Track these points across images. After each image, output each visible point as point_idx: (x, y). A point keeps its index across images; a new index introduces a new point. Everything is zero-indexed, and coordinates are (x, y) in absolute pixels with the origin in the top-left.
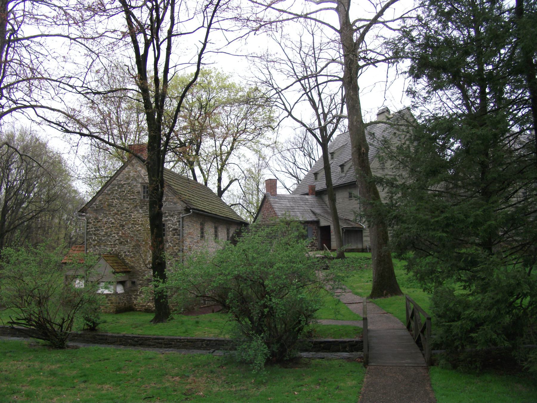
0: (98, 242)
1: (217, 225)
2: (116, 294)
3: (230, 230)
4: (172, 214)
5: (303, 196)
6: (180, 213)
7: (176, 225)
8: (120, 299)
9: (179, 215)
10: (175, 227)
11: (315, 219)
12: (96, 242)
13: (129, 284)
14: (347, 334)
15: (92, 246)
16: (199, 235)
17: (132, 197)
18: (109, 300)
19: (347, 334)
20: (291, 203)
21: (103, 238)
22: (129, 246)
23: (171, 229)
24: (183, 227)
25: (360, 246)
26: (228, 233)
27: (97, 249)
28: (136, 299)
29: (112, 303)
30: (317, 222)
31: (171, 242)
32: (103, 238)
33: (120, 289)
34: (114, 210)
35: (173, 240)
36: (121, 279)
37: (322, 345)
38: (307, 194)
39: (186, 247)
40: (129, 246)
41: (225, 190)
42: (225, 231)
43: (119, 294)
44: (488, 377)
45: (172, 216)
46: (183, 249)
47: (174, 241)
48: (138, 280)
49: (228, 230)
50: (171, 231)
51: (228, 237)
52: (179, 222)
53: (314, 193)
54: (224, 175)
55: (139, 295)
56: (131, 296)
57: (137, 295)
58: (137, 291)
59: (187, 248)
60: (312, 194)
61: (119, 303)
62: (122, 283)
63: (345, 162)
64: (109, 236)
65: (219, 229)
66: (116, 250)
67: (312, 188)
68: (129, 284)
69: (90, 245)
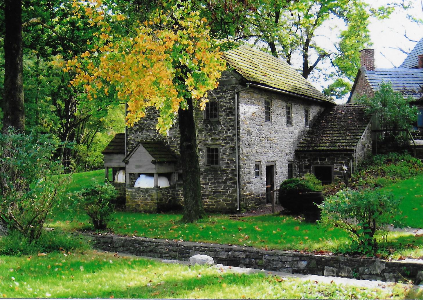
0: (140, 127)
1: (289, 105)
2: (157, 188)
3: (310, 112)
4: (224, 90)
5: (411, 70)
6: (234, 88)
7: (230, 102)
8: (163, 195)
9: (234, 90)
10: (229, 105)
12: (137, 127)
14: (140, 262)
15: (133, 131)
16: (264, 117)
18: (149, 196)
19: (165, 262)
20: (394, 79)
21: (145, 122)
22: (175, 131)
23: (224, 108)
26: (306, 116)
27: (139, 135)
29: (152, 200)
31: (224, 124)
32: (145, 122)
33: (164, 183)
35: (226, 122)
38: (417, 67)
40: (175, 131)
41: (312, 68)
42: (303, 112)
43: (162, 189)
44: (256, 96)
45: (225, 92)
47: (228, 123)
49: (307, 112)
50: (224, 111)
51: (307, 120)
52: (234, 98)
54: (311, 52)
59: (244, 132)
62: (168, 176)
64: (152, 119)
65: (294, 110)
69: (131, 131)
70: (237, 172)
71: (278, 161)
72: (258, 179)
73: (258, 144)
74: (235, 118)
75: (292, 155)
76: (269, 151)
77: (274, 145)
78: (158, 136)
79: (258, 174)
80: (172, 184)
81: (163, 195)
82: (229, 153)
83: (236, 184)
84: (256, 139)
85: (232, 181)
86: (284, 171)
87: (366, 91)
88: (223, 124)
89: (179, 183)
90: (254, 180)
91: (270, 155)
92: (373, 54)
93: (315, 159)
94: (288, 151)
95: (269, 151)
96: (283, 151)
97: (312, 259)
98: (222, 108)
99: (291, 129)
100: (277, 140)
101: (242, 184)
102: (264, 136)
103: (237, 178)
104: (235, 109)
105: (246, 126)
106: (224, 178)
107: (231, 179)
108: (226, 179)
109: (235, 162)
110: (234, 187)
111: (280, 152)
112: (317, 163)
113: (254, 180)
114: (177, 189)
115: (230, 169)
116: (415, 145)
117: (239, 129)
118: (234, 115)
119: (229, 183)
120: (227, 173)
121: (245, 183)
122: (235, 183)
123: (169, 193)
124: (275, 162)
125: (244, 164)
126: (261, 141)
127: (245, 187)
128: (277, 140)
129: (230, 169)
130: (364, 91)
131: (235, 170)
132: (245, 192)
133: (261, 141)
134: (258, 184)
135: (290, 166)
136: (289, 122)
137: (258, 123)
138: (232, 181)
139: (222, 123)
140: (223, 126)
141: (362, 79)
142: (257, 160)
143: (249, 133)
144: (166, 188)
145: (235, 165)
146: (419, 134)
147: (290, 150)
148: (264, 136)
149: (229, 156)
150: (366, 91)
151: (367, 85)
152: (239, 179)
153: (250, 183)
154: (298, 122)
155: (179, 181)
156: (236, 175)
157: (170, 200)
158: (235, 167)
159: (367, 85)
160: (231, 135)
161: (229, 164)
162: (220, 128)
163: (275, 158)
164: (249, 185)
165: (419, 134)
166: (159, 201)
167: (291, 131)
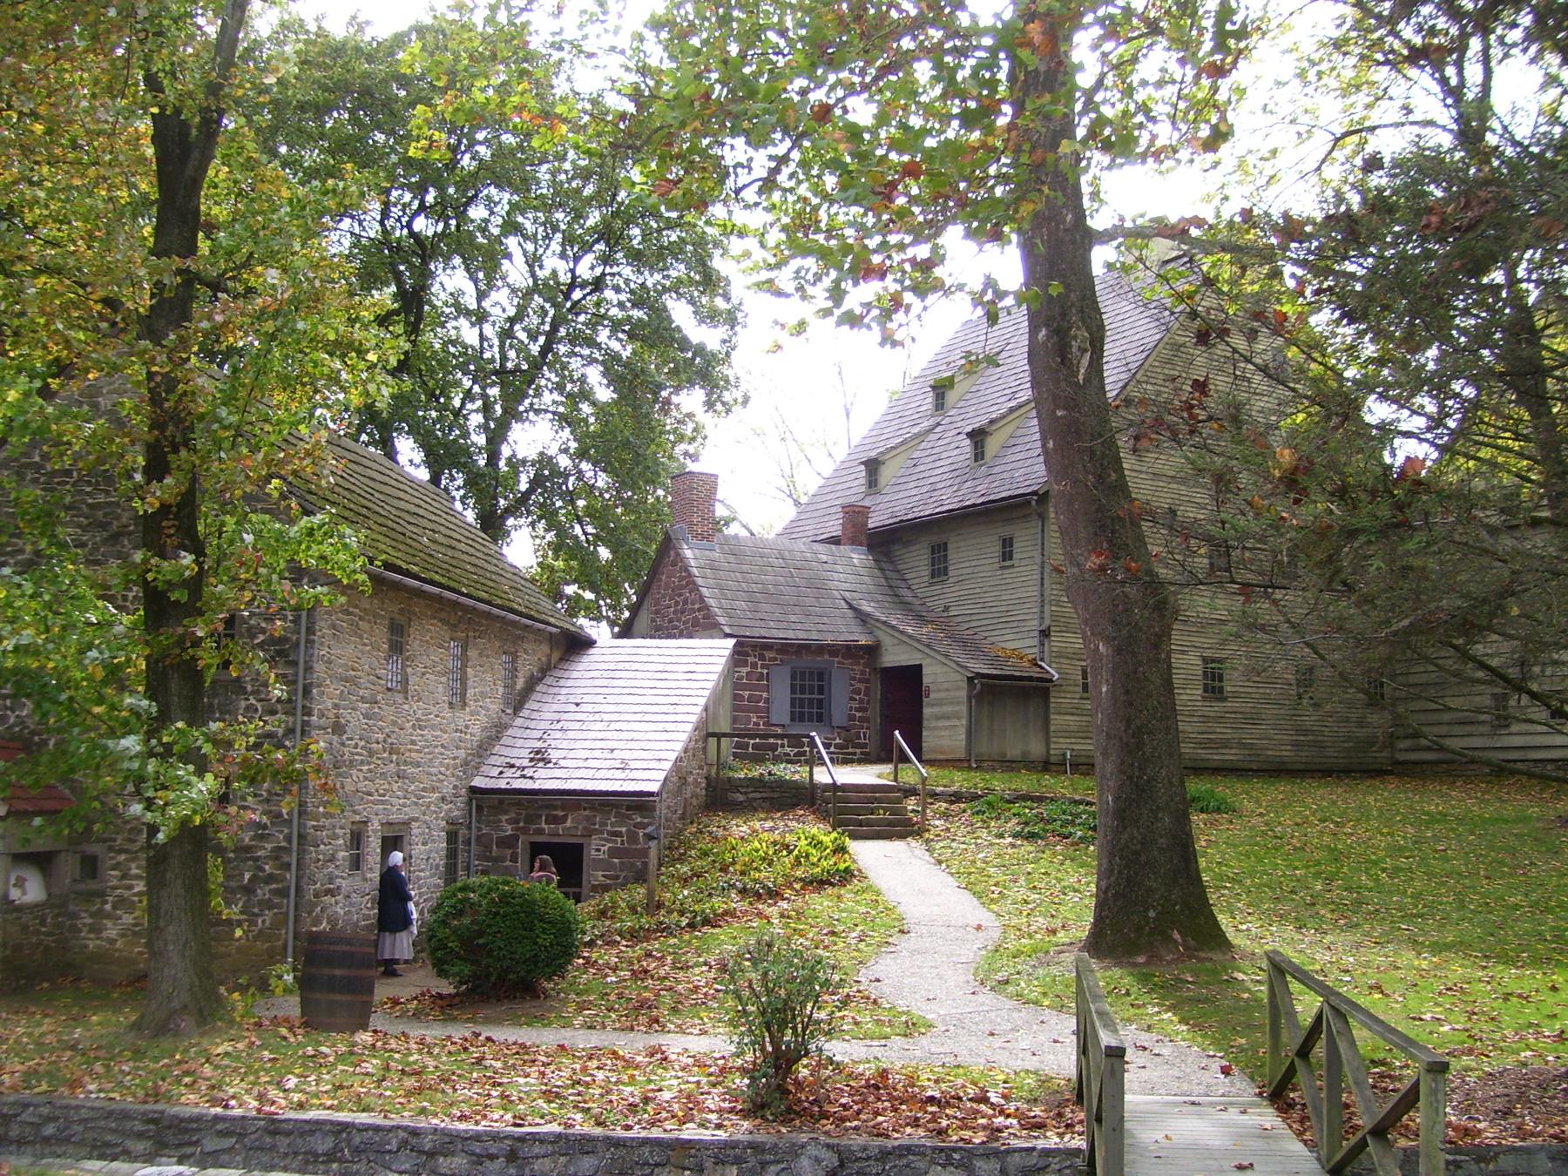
11: (864, 640)
13: (68, 867)
17: (101, 498)
23: (261, 638)
24: (310, 630)
25: (1036, 748)
28: (96, 929)
30: (873, 651)
34: (21, 551)
36: (40, 845)
37: (956, 1156)
38: (835, 541)
39: (322, 715)
46: (305, 724)
48: (111, 849)
53: (863, 538)
55: (108, 916)
56: (75, 916)
57: (100, 914)
58: (101, 894)
60: (854, 542)
61: (18, 948)
62: (42, 861)
63: (992, 422)
66: (21, 722)
67: (854, 516)
68: (68, 867)
70: (294, 855)
71: (416, 820)
72: (357, 882)
73: (362, 763)
74: (296, 674)
75: (461, 802)
76: (395, 787)
77: (410, 770)
78: (12, 720)
79: (356, 863)
80: (55, 891)
81: (25, 928)
82: (269, 792)
83: (288, 896)
84: (356, 746)
85: (274, 886)
86: (434, 855)
87: (685, 602)
88: (253, 693)
89: (82, 887)
90: (344, 883)
91: (394, 801)
92: (716, 483)
93: (530, 819)
94: (447, 789)
95: (395, 787)
96: (433, 790)
97: (783, 1061)
98: (253, 637)
99: (462, 717)
100: (418, 751)
101: (310, 896)
102: (381, 737)
103: (291, 876)
104: (297, 644)
105: (329, 704)
106: (247, 876)
107: (270, 879)
108: (253, 879)
109: (289, 822)
110: (279, 906)
111: (424, 789)
112: (540, 832)
113: (344, 883)
114: (72, 908)
115: (269, 846)
116: (834, 783)
117: (308, 712)
118: (295, 663)
119: (263, 892)
120: (257, 859)
121: (316, 895)
122: (283, 893)
123: (43, 923)
124: (406, 824)
125: (316, 828)
126: (371, 753)
127: (316, 905)
128: (418, 751)
129: (269, 846)
130: (677, 603)
131: (288, 850)
132: (317, 922)
133: (371, 753)
134: (355, 898)
135: (452, 837)
136: (459, 699)
137: (366, 693)
138: (274, 886)
139: (249, 688)
140: (253, 701)
141: (674, 564)
142: (358, 818)
143: (338, 729)
144: (36, 905)
145: (286, 831)
146: (836, 746)
147: (455, 787)
148: (381, 737)
149: (268, 801)
150: (685, 602)
151: (688, 584)
152: (298, 878)
153: (329, 892)
154: (483, 695)
155: (82, 881)
156: (288, 866)
157: (47, 948)
158: (289, 839)
159: (688, 584)
160: (280, 732)
161: (265, 827)
162: (243, 704)
163: (413, 812)
164: (327, 899)
165: (836, 746)
166: (8, 952)
167: (461, 723)
